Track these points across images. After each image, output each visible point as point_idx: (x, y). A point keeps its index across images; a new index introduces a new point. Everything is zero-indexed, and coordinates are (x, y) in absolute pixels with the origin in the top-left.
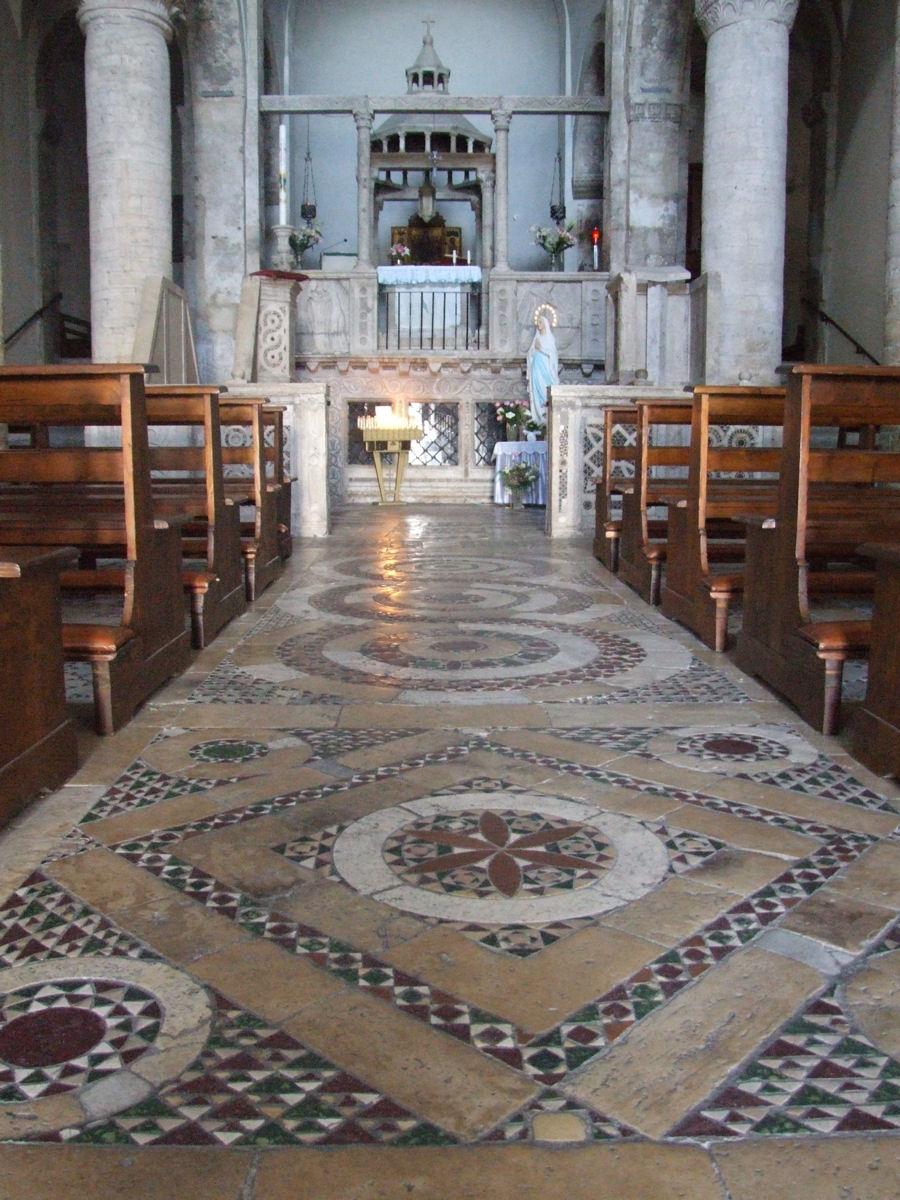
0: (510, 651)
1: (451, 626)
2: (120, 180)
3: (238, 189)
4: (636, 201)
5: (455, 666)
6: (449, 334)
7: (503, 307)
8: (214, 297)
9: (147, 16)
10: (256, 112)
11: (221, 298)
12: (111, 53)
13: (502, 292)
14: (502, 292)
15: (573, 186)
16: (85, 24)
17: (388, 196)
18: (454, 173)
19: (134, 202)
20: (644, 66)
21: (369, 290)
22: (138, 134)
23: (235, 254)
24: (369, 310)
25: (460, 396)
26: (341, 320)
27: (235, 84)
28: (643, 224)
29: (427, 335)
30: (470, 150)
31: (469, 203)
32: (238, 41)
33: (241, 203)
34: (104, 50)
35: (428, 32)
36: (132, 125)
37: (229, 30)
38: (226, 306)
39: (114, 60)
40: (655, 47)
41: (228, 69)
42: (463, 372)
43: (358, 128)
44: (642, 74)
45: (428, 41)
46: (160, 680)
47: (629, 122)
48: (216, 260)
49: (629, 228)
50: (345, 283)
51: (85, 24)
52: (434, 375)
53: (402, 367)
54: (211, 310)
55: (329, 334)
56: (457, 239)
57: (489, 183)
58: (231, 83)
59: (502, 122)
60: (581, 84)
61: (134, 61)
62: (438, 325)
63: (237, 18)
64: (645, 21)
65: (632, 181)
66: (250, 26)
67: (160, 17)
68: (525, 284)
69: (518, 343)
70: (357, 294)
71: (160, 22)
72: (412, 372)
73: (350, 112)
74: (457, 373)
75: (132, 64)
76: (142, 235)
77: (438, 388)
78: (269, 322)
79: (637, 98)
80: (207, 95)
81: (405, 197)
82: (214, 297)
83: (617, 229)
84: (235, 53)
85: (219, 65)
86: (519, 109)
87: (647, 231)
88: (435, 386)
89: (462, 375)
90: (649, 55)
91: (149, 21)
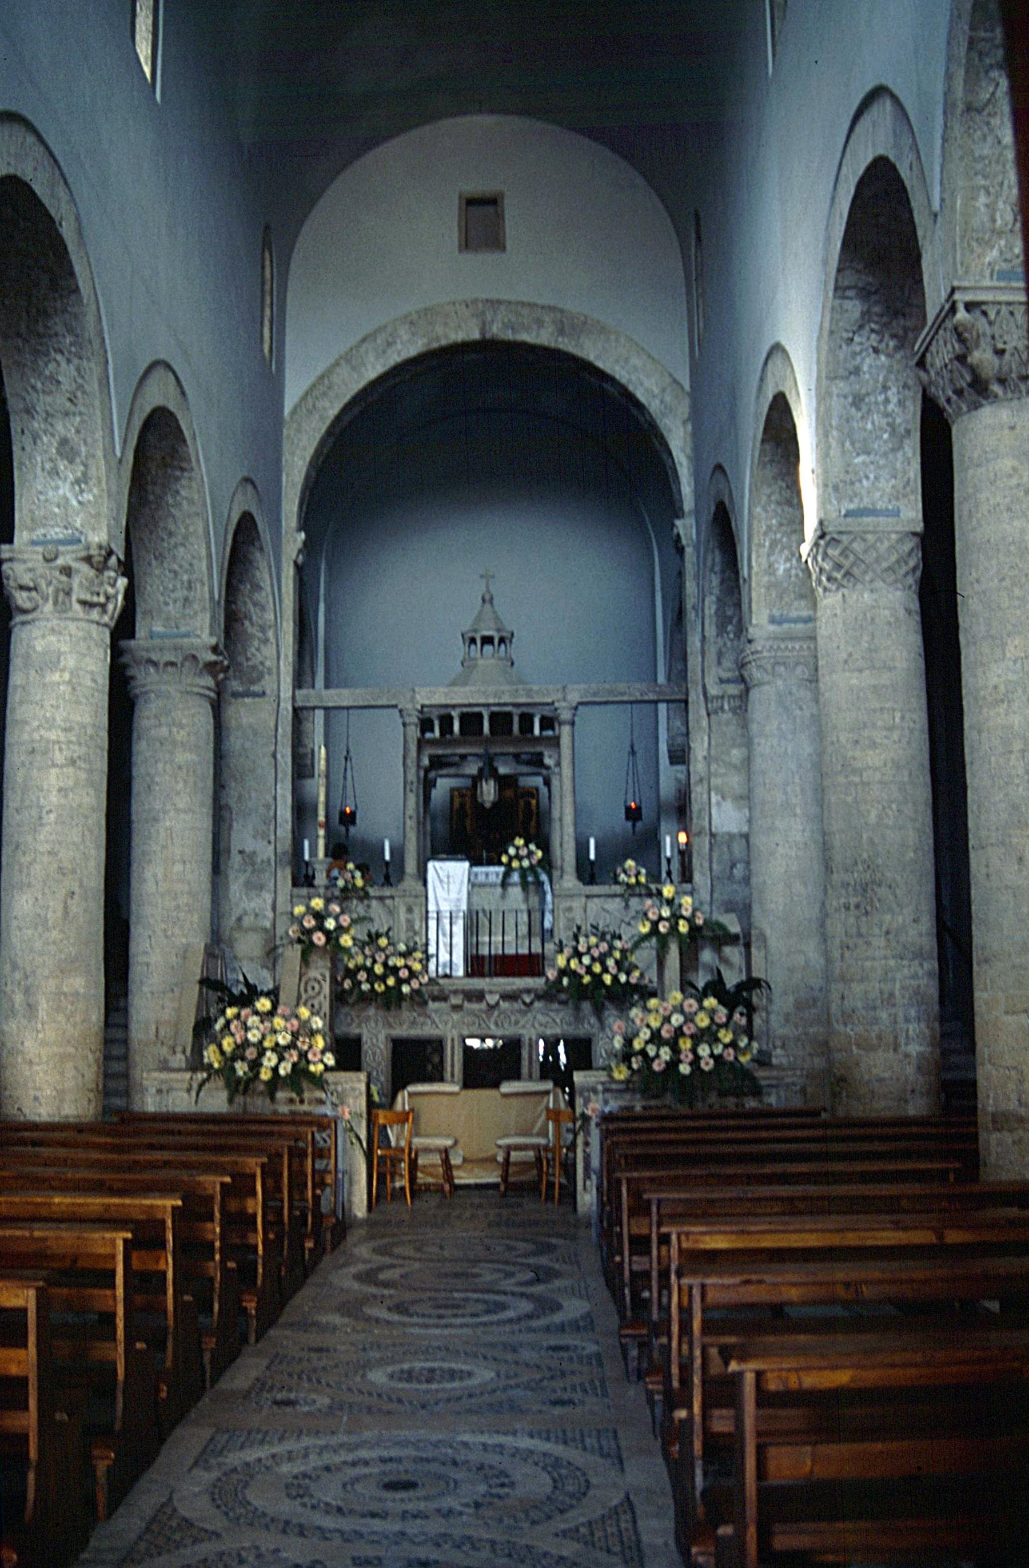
0: (480, 1307)
1: (448, 1295)
2: (164, 847)
3: (269, 798)
4: (718, 804)
5: (440, 1317)
8: (239, 919)
9: (196, 690)
10: (290, 709)
11: (247, 921)
12: (160, 725)
13: (570, 909)
14: (570, 909)
15: (669, 751)
16: (137, 696)
17: (444, 772)
19: (178, 867)
20: (720, 655)
22: (182, 802)
23: (263, 871)
25: (521, 1031)
27: (267, 684)
28: (725, 829)
32: (273, 640)
33: (272, 813)
34: (152, 721)
35: (487, 587)
36: (178, 793)
37: (263, 629)
38: (253, 929)
39: (164, 731)
40: (732, 636)
41: (261, 668)
42: (524, 1003)
43: (404, 725)
44: (719, 663)
45: (487, 597)
46: (272, 1323)
47: (709, 715)
48: (242, 878)
49: (713, 835)
50: (388, 902)
51: (137, 696)
52: (492, 1008)
53: (455, 1000)
54: (236, 935)
56: (534, 802)
58: (263, 683)
60: (672, 635)
61: (182, 732)
63: (272, 617)
64: (718, 610)
65: (714, 781)
66: (285, 617)
67: (209, 689)
68: (596, 900)
71: (207, 692)
72: (466, 1004)
73: (395, 706)
74: (518, 1005)
75: (180, 735)
76: (183, 900)
77: (496, 1024)
78: (309, 989)
79: (713, 691)
80: (236, 695)
81: (461, 772)
82: (239, 919)
84: (269, 651)
85: (250, 663)
86: (585, 700)
87: (731, 836)
88: (493, 1020)
89: (523, 1007)
90: (725, 644)
91: (198, 694)
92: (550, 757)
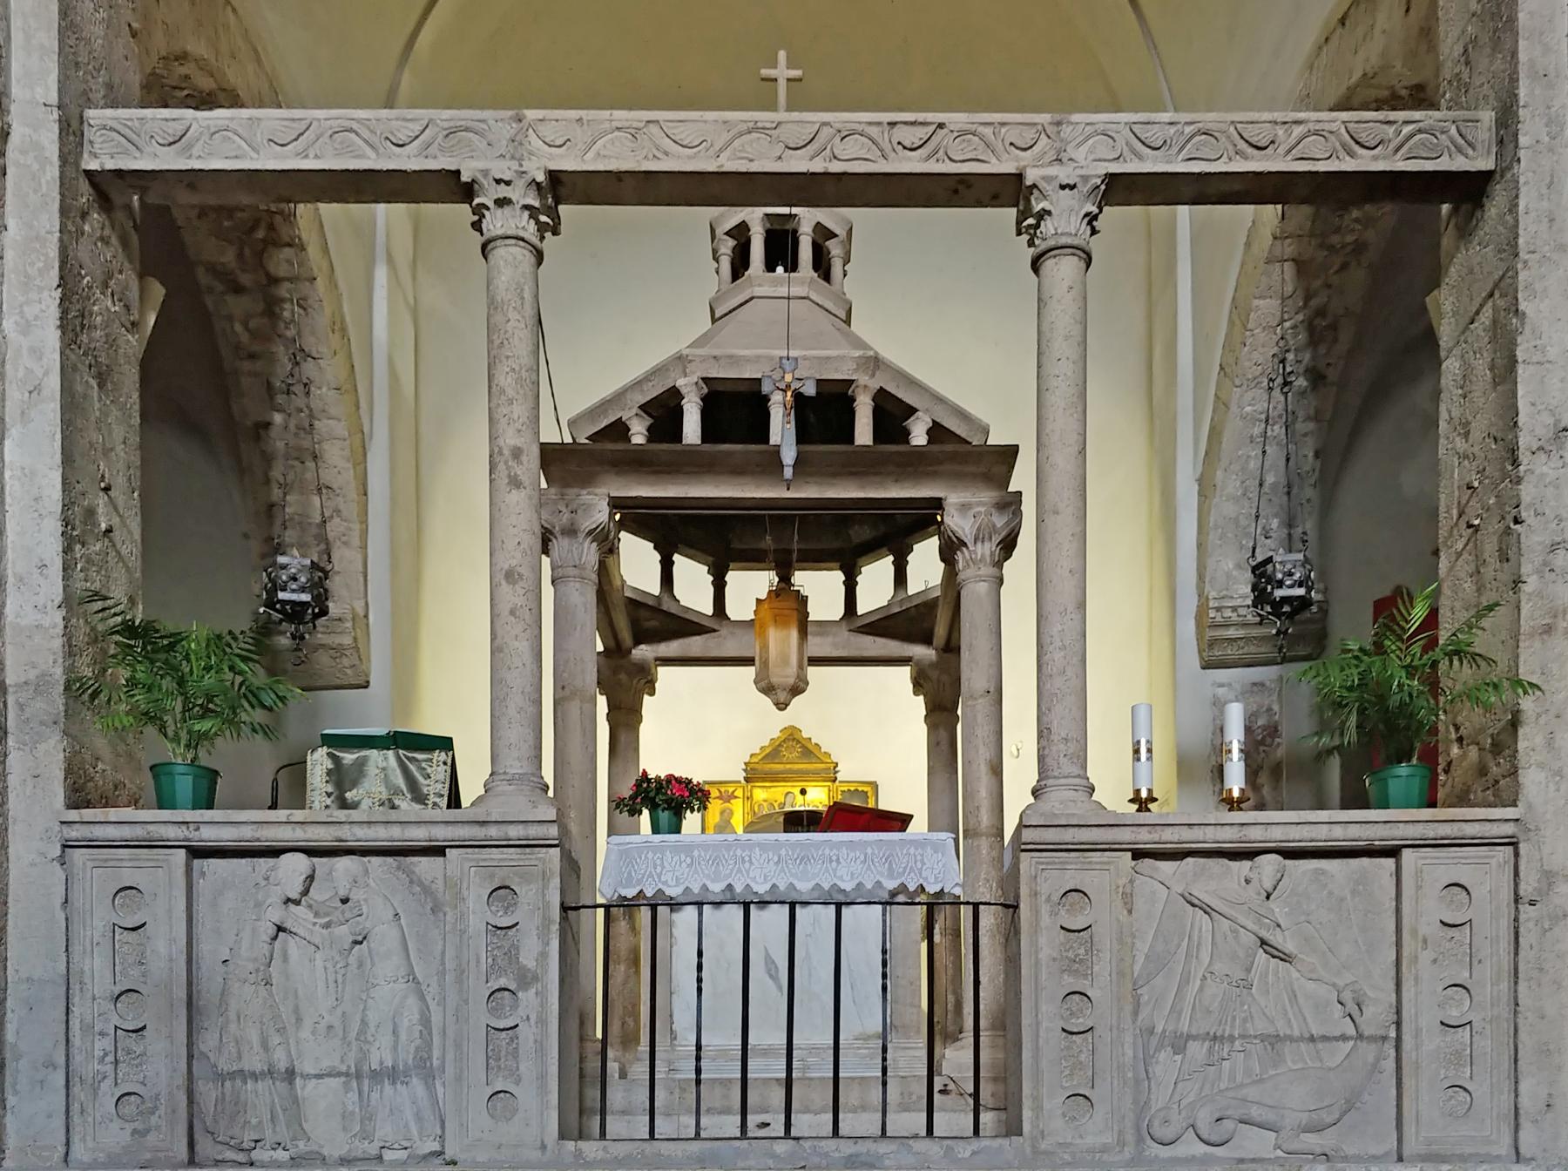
6: (859, 1065)
7: (1075, 965)
18: (844, 909)
21: (527, 894)
24: (527, 979)
26: (411, 1014)
29: (767, 1068)
30: (919, 437)
31: (905, 672)
55: (359, 1075)
57: (986, 549)
59: (1064, 218)
62: (813, 1033)
69: (1142, 1107)
70: (477, 912)
83: (1548, 630)
92: (964, 508)
